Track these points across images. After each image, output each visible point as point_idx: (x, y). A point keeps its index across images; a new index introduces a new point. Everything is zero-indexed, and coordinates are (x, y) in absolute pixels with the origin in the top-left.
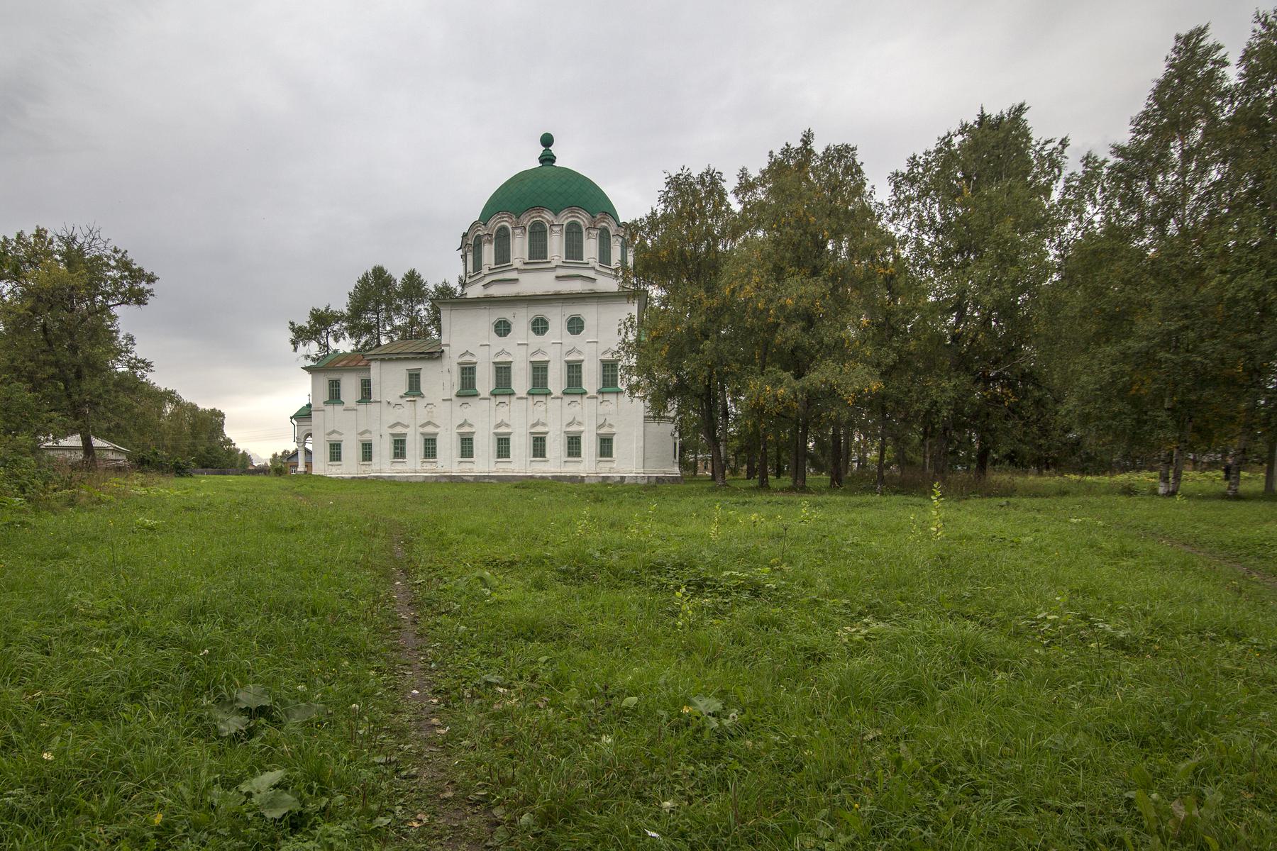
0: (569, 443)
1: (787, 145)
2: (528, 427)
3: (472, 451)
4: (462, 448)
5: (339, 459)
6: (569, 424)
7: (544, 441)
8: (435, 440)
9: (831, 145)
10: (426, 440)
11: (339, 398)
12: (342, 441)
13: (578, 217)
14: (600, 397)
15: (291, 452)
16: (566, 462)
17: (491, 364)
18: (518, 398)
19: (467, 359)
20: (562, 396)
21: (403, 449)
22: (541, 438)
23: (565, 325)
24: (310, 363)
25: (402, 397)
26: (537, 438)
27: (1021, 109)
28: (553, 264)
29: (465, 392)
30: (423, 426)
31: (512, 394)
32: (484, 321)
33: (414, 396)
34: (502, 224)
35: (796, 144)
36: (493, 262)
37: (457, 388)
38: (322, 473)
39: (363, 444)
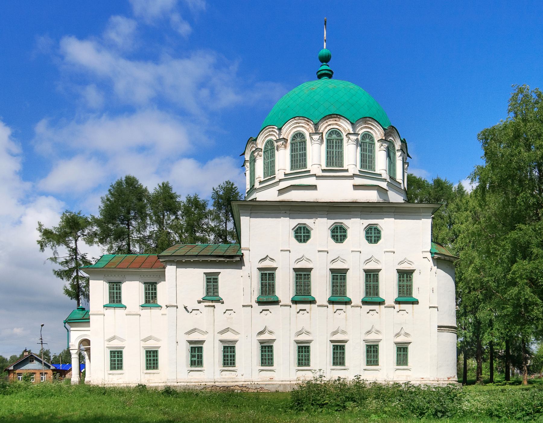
0: (368, 351)
1: (196, 194)
2: (329, 335)
3: (272, 359)
4: (262, 355)
5: (120, 367)
6: (369, 332)
7: (344, 349)
8: (234, 347)
9: (59, 223)
10: (225, 347)
11: (120, 301)
12: (379, 341)
13: (371, 129)
14: (397, 306)
15: (18, 356)
16: (365, 370)
17: (292, 270)
18: (319, 306)
19: (267, 264)
20: (291, 304)
21: (200, 357)
22: (340, 346)
23: (363, 234)
24: (59, 267)
25: (199, 302)
26: (337, 346)
27: (349, 269)
28: (350, 173)
29: (265, 299)
30: (222, 332)
31: (313, 302)
32: (469, 374)
33: (212, 301)
34: (298, 129)
35: (66, 349)
36: (262, 175)
37: (256, 294)
38: (249, 158)
39: (147, 352)
